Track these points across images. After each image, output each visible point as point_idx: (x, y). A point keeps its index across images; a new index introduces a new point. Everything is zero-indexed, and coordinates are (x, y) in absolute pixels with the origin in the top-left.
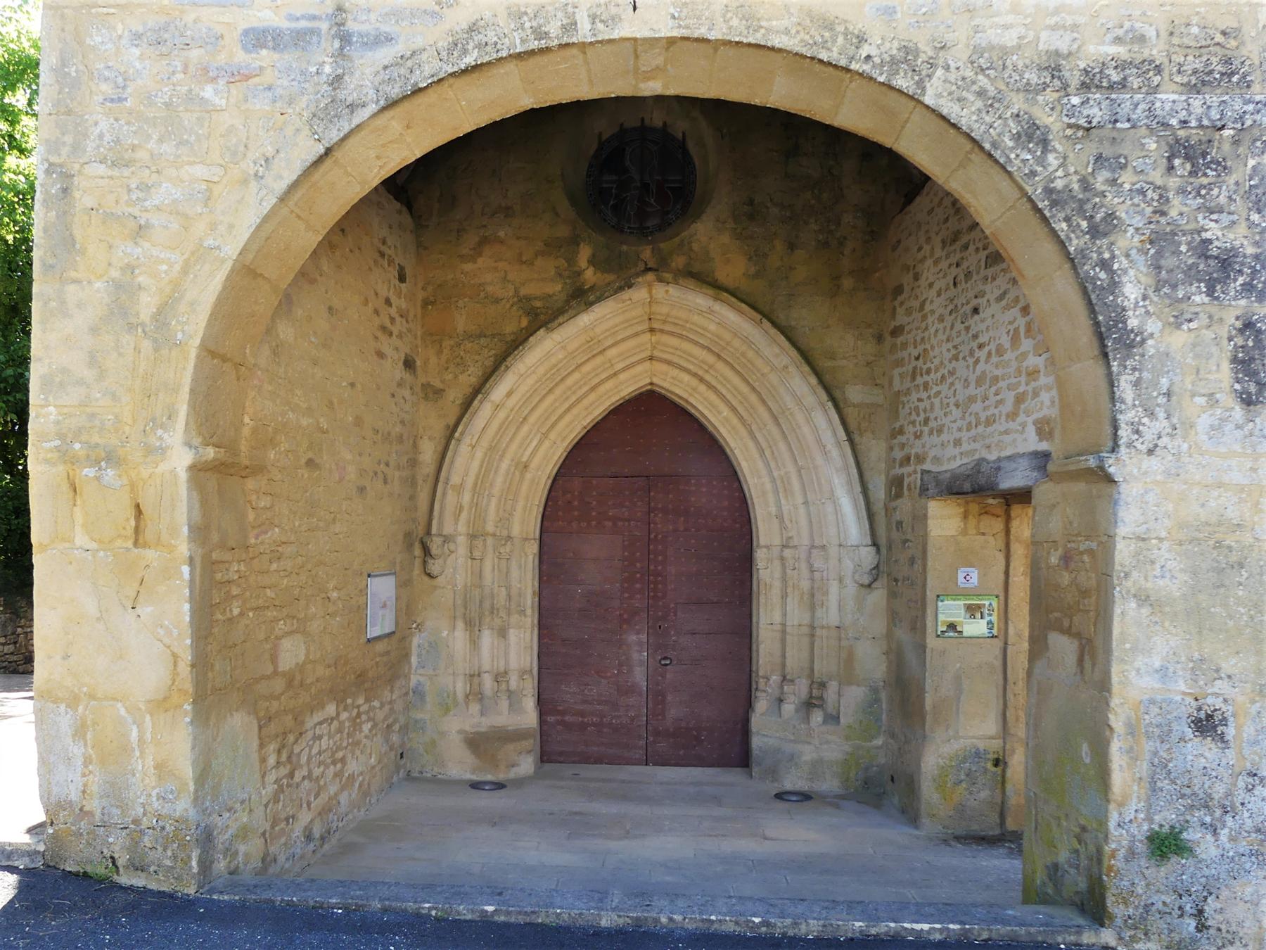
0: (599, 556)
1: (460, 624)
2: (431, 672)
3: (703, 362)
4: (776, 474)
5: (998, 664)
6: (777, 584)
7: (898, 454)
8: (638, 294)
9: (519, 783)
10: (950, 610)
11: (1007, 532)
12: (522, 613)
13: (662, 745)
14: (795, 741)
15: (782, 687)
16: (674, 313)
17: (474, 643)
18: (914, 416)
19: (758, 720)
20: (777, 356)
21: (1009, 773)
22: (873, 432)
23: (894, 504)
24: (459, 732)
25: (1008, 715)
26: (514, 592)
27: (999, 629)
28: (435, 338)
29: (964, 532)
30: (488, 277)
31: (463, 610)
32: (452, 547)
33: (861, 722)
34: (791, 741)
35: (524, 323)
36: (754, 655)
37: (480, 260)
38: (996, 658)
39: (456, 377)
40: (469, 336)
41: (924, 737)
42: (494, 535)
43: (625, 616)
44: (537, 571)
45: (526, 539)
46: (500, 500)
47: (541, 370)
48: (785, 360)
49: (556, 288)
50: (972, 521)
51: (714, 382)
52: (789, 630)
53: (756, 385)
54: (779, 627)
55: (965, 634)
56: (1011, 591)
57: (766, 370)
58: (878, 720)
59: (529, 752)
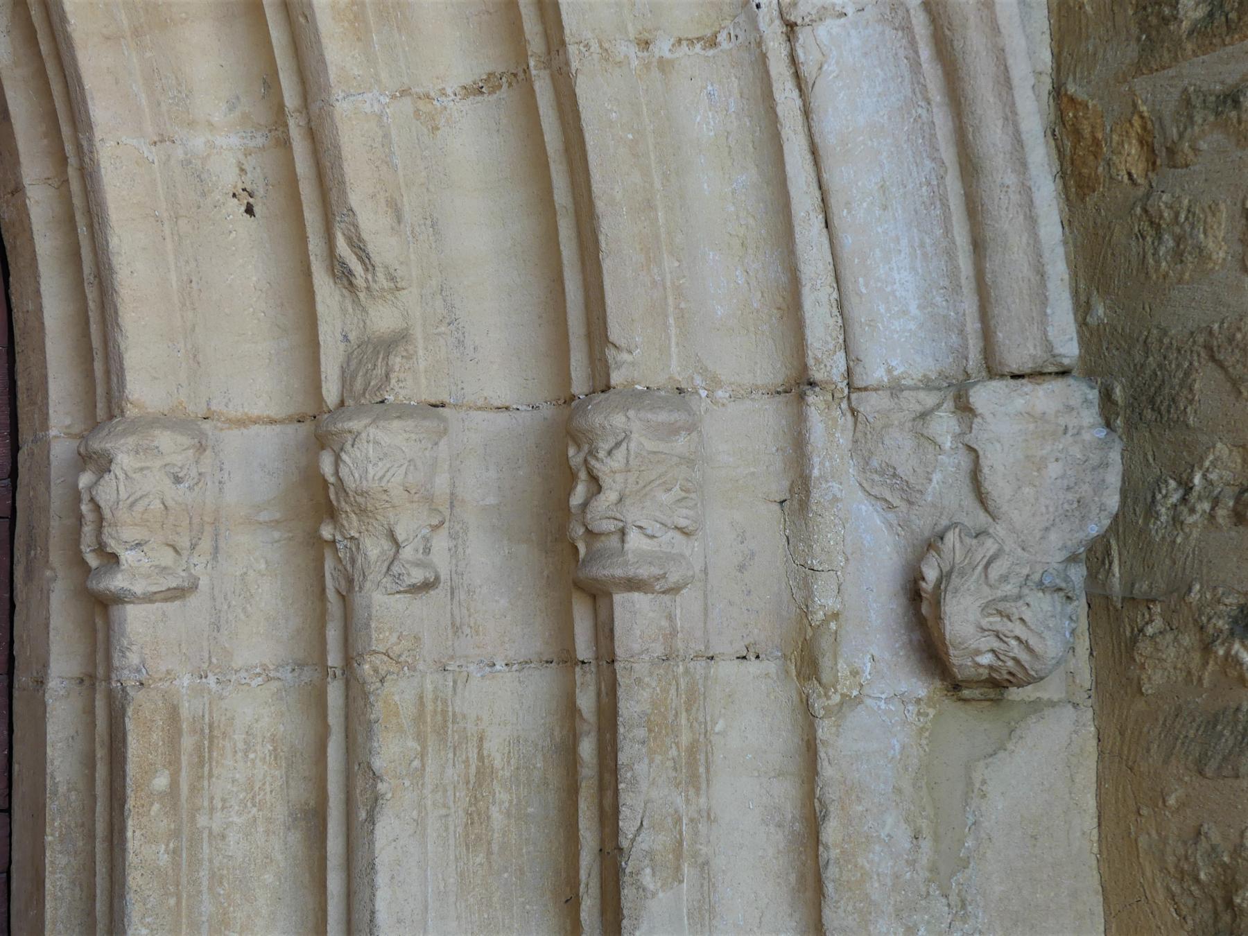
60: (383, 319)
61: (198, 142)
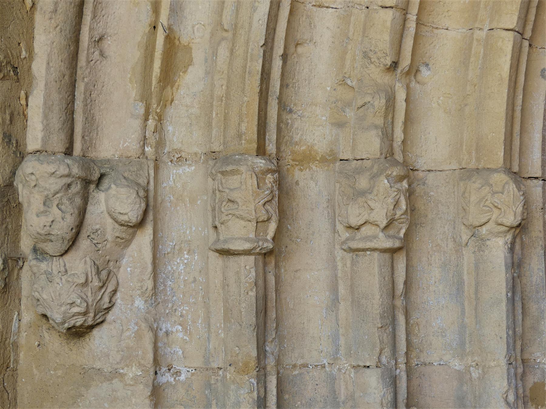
42: (330, 159)
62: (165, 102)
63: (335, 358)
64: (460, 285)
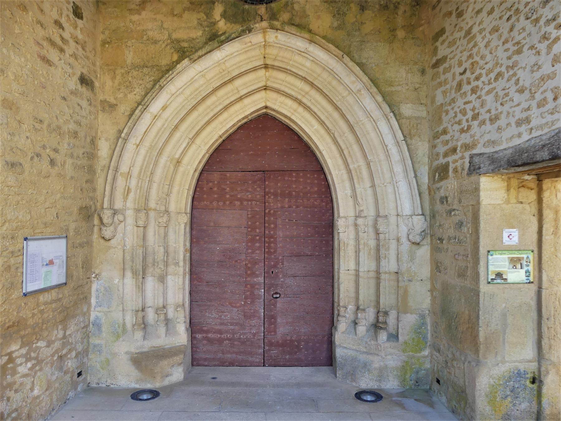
0: (230, 224)
1: (129, 274)
2: (106, 309)
3: (301, 89)
4: (351, 167)
5: (533, 303)
6: (352, 243)
7: (441, 149)
8: (256, 38)
9: (171, 389)
10: (498, 262)
11: (540, 201)
12: (177, 264)
13: (274, 352)
14: (367, 353)
15: (357, 314)
16: (281, 54)
17: (141, 288)
18: (460, 116)
19: (339, 337)
20: (353, 83)
21: (545, 390)
22: (419, 136)
23: (438, 185)
24: (127, 353)
25: (543, 343)
26: (171, 249)
27: (534, 277)
28: (111, 68)
29: (508, 202)
30: (150, 25)
31: (130, 263)
32: (121, 218)
33: (413, 339)
34: (364, 353)
35: (175, 57)
36: (336, 291)
37: (144, 13)
38: (532, 299)
39: (126, 95)
40: (135, 67)
41: (478, 363)
42: (155, 210)
43: (249, 265)
44: (188, 235)
45: (179, 213)
46: (159, 185)
47: (188, 92)
48: (359, 86)
49: (198, 34)
50: (513, 192)
51: (309, 104)
52: (361, 274)
53: (338, 104)
54: (353, 272)
55: (509, 281)
56: (544, 247)
57: (345, 94)
58: (425, 338)
59: (180, 364)
60: (361, 208)
61: (346, 192)
62: (127, 199)
63: (154, 244)
64: (176, 232)
